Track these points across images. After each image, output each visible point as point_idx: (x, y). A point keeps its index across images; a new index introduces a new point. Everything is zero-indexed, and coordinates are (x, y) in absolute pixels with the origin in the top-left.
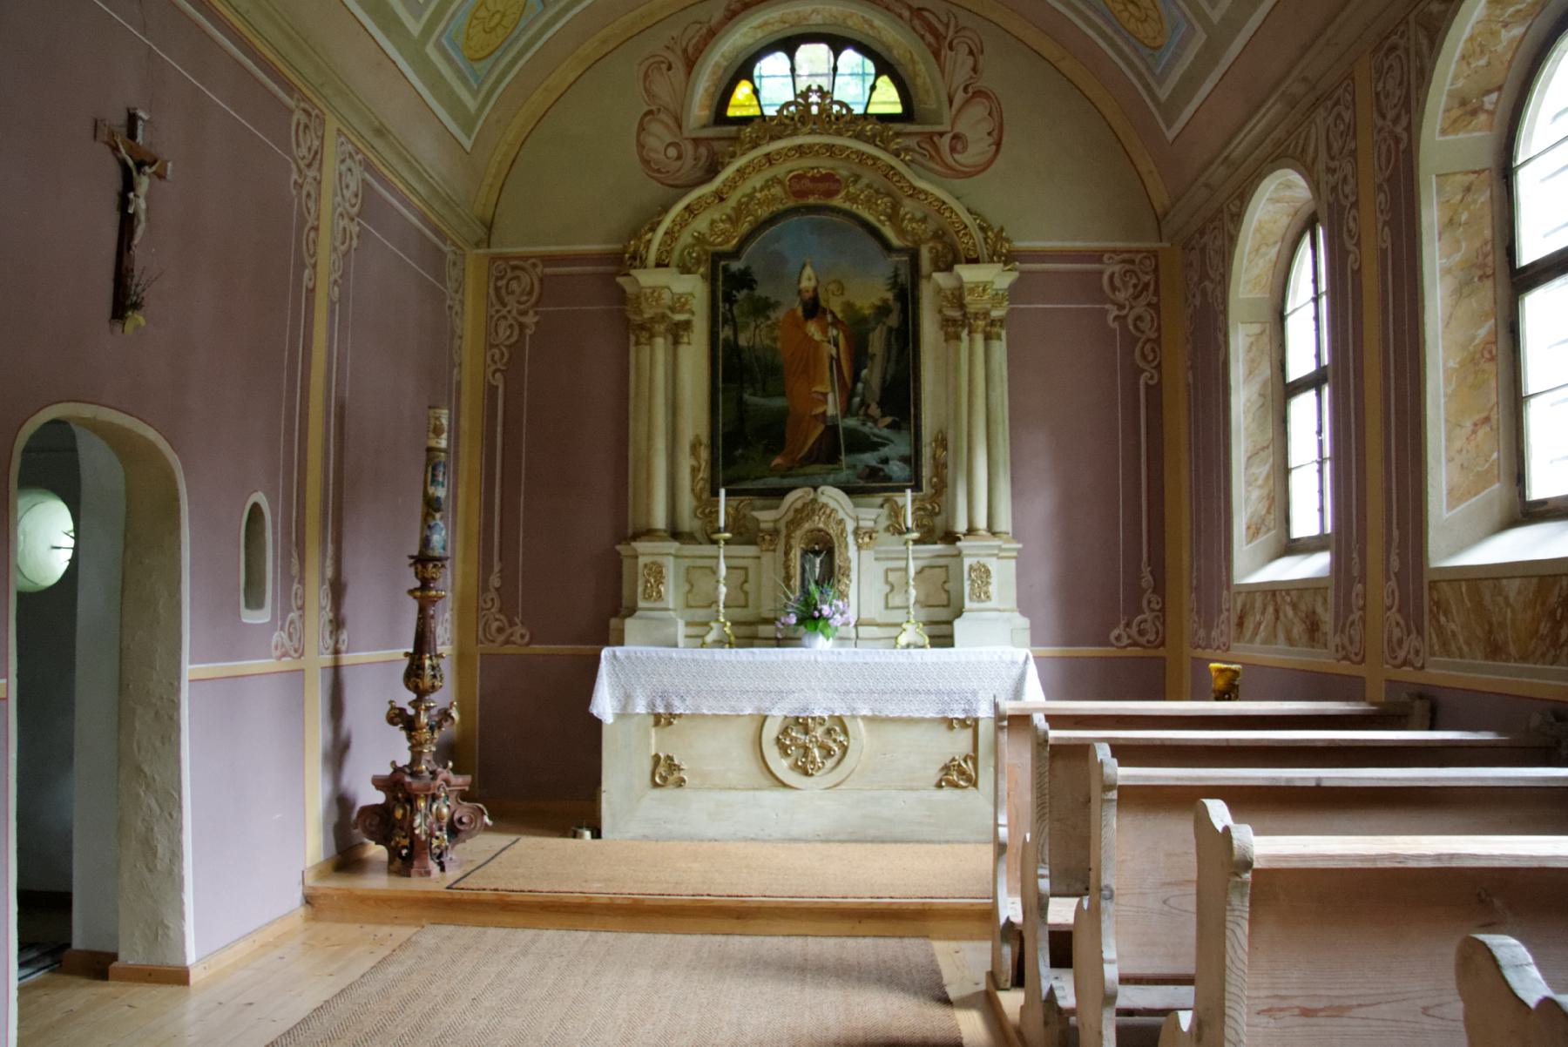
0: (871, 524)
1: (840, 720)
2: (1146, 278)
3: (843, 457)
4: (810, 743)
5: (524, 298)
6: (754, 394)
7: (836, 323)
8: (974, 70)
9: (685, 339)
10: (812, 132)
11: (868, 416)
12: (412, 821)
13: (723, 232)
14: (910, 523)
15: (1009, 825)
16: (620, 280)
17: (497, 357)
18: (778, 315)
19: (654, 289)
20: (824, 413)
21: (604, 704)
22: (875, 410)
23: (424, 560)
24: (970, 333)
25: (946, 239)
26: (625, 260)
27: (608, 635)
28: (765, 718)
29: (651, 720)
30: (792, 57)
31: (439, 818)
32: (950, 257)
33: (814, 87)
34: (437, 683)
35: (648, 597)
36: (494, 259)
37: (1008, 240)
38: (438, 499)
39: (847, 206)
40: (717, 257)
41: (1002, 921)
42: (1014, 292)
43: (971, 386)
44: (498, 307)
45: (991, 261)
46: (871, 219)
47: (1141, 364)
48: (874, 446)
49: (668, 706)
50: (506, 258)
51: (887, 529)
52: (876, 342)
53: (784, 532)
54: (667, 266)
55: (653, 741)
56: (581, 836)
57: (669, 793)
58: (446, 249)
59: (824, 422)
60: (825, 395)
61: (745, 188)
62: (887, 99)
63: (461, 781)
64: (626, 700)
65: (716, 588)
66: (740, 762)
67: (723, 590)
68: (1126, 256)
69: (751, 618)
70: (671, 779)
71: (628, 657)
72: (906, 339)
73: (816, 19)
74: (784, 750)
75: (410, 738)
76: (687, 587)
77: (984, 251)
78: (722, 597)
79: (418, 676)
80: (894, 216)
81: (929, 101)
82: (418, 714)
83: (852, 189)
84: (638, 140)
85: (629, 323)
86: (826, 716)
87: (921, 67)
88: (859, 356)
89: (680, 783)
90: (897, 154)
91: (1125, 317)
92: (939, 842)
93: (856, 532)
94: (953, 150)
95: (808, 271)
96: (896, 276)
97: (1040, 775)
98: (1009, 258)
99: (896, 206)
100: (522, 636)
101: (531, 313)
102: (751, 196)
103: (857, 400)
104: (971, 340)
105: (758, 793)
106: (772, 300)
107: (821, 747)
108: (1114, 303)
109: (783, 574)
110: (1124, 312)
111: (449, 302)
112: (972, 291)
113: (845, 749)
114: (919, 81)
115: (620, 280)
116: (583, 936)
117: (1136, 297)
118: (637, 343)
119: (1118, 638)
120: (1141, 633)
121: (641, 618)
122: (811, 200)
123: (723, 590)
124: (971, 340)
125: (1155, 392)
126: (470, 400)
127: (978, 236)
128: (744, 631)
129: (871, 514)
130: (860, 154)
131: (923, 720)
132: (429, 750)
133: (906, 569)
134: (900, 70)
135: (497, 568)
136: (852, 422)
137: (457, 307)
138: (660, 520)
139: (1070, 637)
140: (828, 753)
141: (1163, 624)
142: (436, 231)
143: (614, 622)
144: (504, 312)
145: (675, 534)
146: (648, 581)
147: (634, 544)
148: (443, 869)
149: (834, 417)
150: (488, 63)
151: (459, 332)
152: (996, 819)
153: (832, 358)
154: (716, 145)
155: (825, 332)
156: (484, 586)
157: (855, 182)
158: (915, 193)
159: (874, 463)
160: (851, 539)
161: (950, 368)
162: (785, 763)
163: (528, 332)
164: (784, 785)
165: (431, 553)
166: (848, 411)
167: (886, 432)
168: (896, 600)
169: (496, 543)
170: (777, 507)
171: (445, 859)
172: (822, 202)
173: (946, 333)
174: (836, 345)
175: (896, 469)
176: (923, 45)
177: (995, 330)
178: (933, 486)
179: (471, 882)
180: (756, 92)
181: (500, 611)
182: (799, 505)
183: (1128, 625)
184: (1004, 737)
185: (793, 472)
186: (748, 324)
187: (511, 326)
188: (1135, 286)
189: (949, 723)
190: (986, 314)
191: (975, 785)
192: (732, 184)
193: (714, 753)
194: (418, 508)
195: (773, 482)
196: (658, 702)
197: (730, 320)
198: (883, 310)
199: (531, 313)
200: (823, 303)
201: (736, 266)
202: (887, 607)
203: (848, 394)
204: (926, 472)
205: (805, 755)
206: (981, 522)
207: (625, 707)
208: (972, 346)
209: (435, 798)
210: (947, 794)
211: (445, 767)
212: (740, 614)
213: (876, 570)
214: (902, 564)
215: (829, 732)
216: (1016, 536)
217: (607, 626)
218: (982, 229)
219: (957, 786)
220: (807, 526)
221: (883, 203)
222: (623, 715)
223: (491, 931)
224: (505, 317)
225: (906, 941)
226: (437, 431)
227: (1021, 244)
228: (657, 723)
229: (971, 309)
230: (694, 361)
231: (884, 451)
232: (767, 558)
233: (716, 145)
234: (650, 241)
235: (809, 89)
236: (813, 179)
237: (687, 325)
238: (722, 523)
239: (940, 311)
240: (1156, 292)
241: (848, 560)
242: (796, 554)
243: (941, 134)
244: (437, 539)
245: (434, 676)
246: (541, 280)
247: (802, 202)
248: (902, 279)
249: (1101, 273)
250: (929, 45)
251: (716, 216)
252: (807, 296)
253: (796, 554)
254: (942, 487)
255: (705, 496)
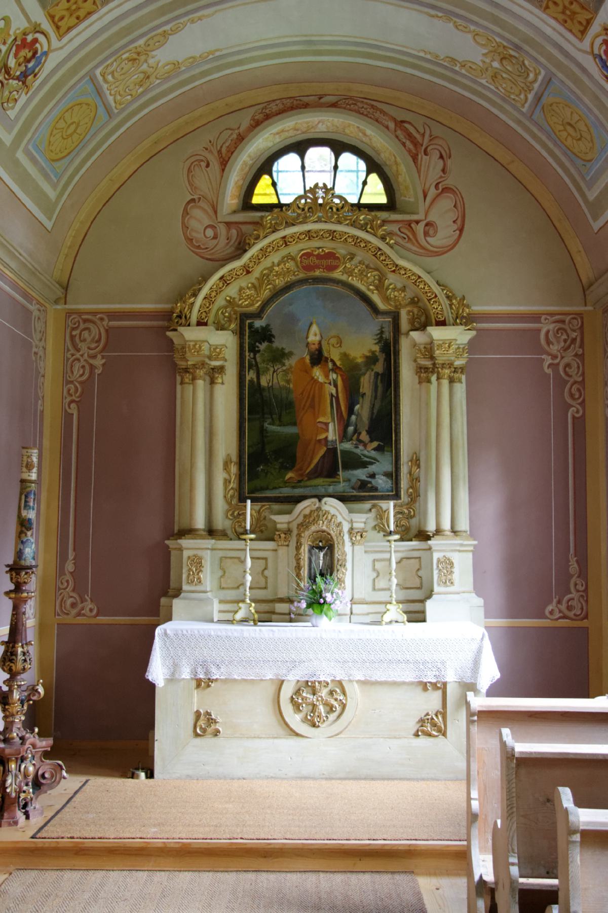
0: (362, 525)
1: (340, 683)
2: (574, 335)
3: (340, 473)
4: (315, 702)
5: (93, 345)
6: (273, 424)
7: (336, 369)
8: (444, 171)
9: (220, 380)
10: (319, 220)
11: (360, 441)
12: (5, 781)
13: (249, 297)
14: (392, 528)
15: (479, 800)
16: (170, 334)
17: (72, 391)
18: (291, 362)
19: (196, 342)
20: (327, 438)
21: (157, 672)
22: (364, 436)
23: (17, 569)
24: (438, 378)
25: (420, 304)
26: (173, 319)
27: (158, 612)
28: (283, 682)
29: (194, 683)
30: (302, 157)
31: (26, 776)
32: (423, 319)
33: (321, 185)
34: (27, 666)
35: (190, 582)
36: (69, 313)
37: (468, 306)
38: (29, 520)
39: (344, 278)
40: (244, 317)
41: (477, 878)
42: (472, 346)
43: (439, 418)
44: (72, 351)
45: (455, 324)
46: (363, 288)
47: (569, 400)
48: (364, 465)
49: (207, 673)
50: (79, 313)
51: (374, 528)
52: (366, 383)
53: (295, 532)
54: (205, 324)
55: (195, 700)
56: (138, 777)
57: (208, 741)
58: (33, 307)
59: (326, 445)
60: (327, 424)
61: (266, 263)
62: (376, 193)
63: (45, 744)
64: (175, 668)
65: (244, 577)
66: (263, 715)
67: (249, 578)
68: (557, 317)
69: (271, 598)
70: (209, 730)
71: (176, 635)
72: (389, 381)
73: (322, 128)
74: (297, 707)
75: (4, 710)
76: (220, 573)
77: (449, 315)
78: (248, 584)
79: (11, 661)
80: (380, 287)
81: (407, 196)
82: (11, 690)
83: (348, 265)
84: (183, 223)
85: (175, 367)
86: (329, 680)
87: (403, 168)
88: (353, 394)
89: (216, 733)
90: (383, 238)
91: (558, 364)
92: (417, 780)
93: (351, 530)
94: (426, 234)
95: (314, 328)
96: (382, 332)
97: (509, 782)
98: (467, 320)
99: (382, 278)
100: (91, 610)
101: (99, 356)
102: (271, 269)
103: (351, 429)
104: (439, 385)
105: (276, 741)
106: (286, 351)
107: (326, 704)
108: (549, 354)
109: (295, 564)
110: (556, 361)
111: (34, 350)
112: (440, 346)
113: (344, 706)
114: (400, 179)
115: (170, 334)
116: (142, 876)
117: (566, 349)
118: (182, 383)
119: (551, 612)
120: (569, 608)
121: (185, 598)
122: (317, 273)
123: (249, 578)
124: (439, 385)
125: (580, 424)
126: (50, 438)
127: (445, 302)
128: (265, 607)
129: (362, 519)
130: (356, 238)
131: (404, 683)
132: (19, 719)
133: (390, 560)
134: (386, 169)
135: (71, 557)
136: (347, 446)
137: (41, 353)
138: (200, 522)
139: (513, 608)
140: (331, 709)
141: (587, 601)
142: (25, 295)
143: (163, 600)
144: (78, 355)
145: (211, 532)
146: (190, 570)
147: (179, 541)
148: (28, 817)
149: (334, 442)
150: (66, 161)
151: (42, 372)
152: (469, 793)
153: (332, 395)
154: (244, 228)
155: (327, 376)
156: (61, 571)
157: (352, 259)
158: (397, 269)
159: (364, 478)
160: (346, 537)
161: (422, 406)
162: (298, 717)
163: (98, 371)
164: (297, 735)
165: (23, 563)
166: (344, 437)
167: (374, 454)
168: (381, 584)
169: (72, 537)
170: (289, 512)
171: (30, 808)
172: (326, 274)
173: (420, 377)
174: (336, 386)
175: (382, 482)
176: (406, 153)
177: (456, 375)
178: (410, 495)
179: (52, 831)
180: (274, 184)
181: (73, 590)
182: (307, 512)
183: (559, 602)
184: (475, 729)
185: (302, 484)
186: (268, 369)
187: (83, 367)
188: (565, 341)
189: (424, 686)
190: (451, 365)
191: (444, 734)
192: (257, 260)
193: (244, 711)
194: (12, 528)
195: (286, 491)
196: (199, 670)
197: (254, 366)
198: (371, 360)
199: (99, 356)
200: (326, 354)
201: (258, 324)
202: (374, 589)
203: (344, 424)
204: (404, 483)
205: (313, 711)
206: (446, 525)
207: (173, 674)
208: (440, 389)
209: (23, 759)
210: (423, 741)
211: (32, 731)
212: (261, 594)
213: (366, 559)
214: (387, 556)
215: (331, 693)
216: (472, 535)
217: (159, 602)
218: (448, 297)
219: (430, 735)
220: (313, 528)
221: (372, 275)
222: (172, 680)
223: (68, 875)
224: (78, 360)
225: (397, 877)
226: (29, 467)
227: (477, 308)
228: (198, 686)
229: (440, 360)
230: (226, 396)
231: (372, 469)
232: (282, 551)
233: (244, 228)
234: (193, 304)
235: (316, 185)
236: (319, 257)
237: (221, 369)
238: (248, 527)
239: (415, 361)
240: (582, 346)
241: (344, 554)
242: (305, 549)
243: (417, 222)
244: (28, 551)
245: (25, 661)
246: (107, 331)
247: (311, 274)
248: (386, 335)
249: (539, 330)
250: (409, 151)
251: (244, 285)
252: (314, 347)
253: (305, 549)
254: (415, 496)
255: (234, 502)
